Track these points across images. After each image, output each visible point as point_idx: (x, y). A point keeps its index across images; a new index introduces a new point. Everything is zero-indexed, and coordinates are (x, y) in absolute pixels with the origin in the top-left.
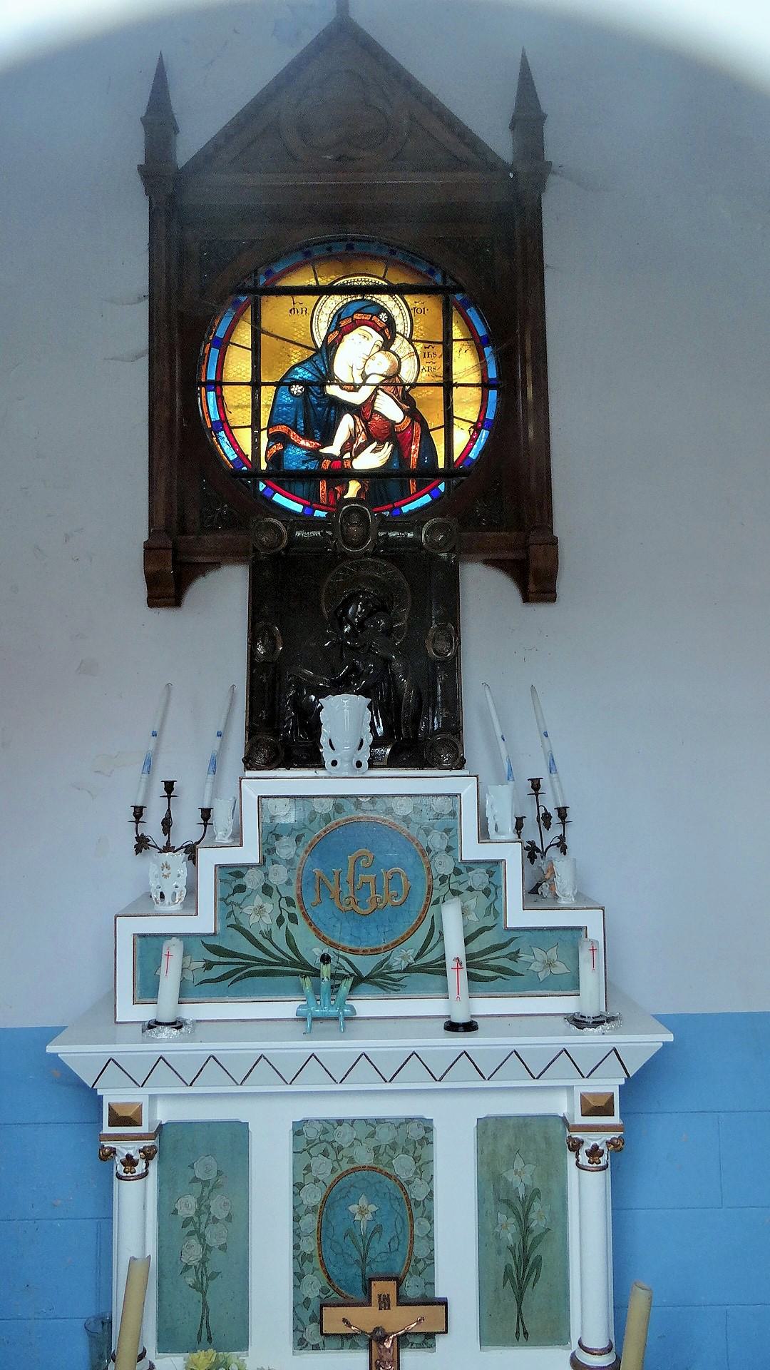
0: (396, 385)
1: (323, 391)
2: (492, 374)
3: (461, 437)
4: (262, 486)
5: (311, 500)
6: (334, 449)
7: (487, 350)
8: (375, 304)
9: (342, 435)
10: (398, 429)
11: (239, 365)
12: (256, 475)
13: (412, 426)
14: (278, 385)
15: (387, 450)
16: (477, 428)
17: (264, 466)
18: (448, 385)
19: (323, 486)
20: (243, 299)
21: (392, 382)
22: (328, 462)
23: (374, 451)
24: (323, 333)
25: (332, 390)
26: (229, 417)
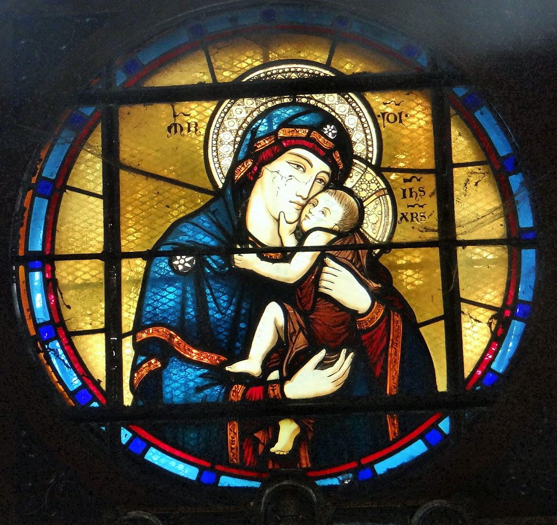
0: (355, 248)
1: (230, 261)
2: (526, 221)
3: (475, 337)
4: (125, 436)
5: (212, 459)
6: (251, 365)
7: (515, 181)
8: (314, 109)
9: (264, 338)
10: (365, 324)
11: (82, 222)
12: (117, 415)
13: (386, 318)
14: (148, 256)
15: (344, 363)
16: (501, 320)
17: (128, 399)
18: (447, 242)
19: (233, 433)
20: (89, 111)
21: (348, 243)
22: (240, 389)
23: (322, 366)
24: (227, 163)
25: (248, 261)
26: (67, 314)
